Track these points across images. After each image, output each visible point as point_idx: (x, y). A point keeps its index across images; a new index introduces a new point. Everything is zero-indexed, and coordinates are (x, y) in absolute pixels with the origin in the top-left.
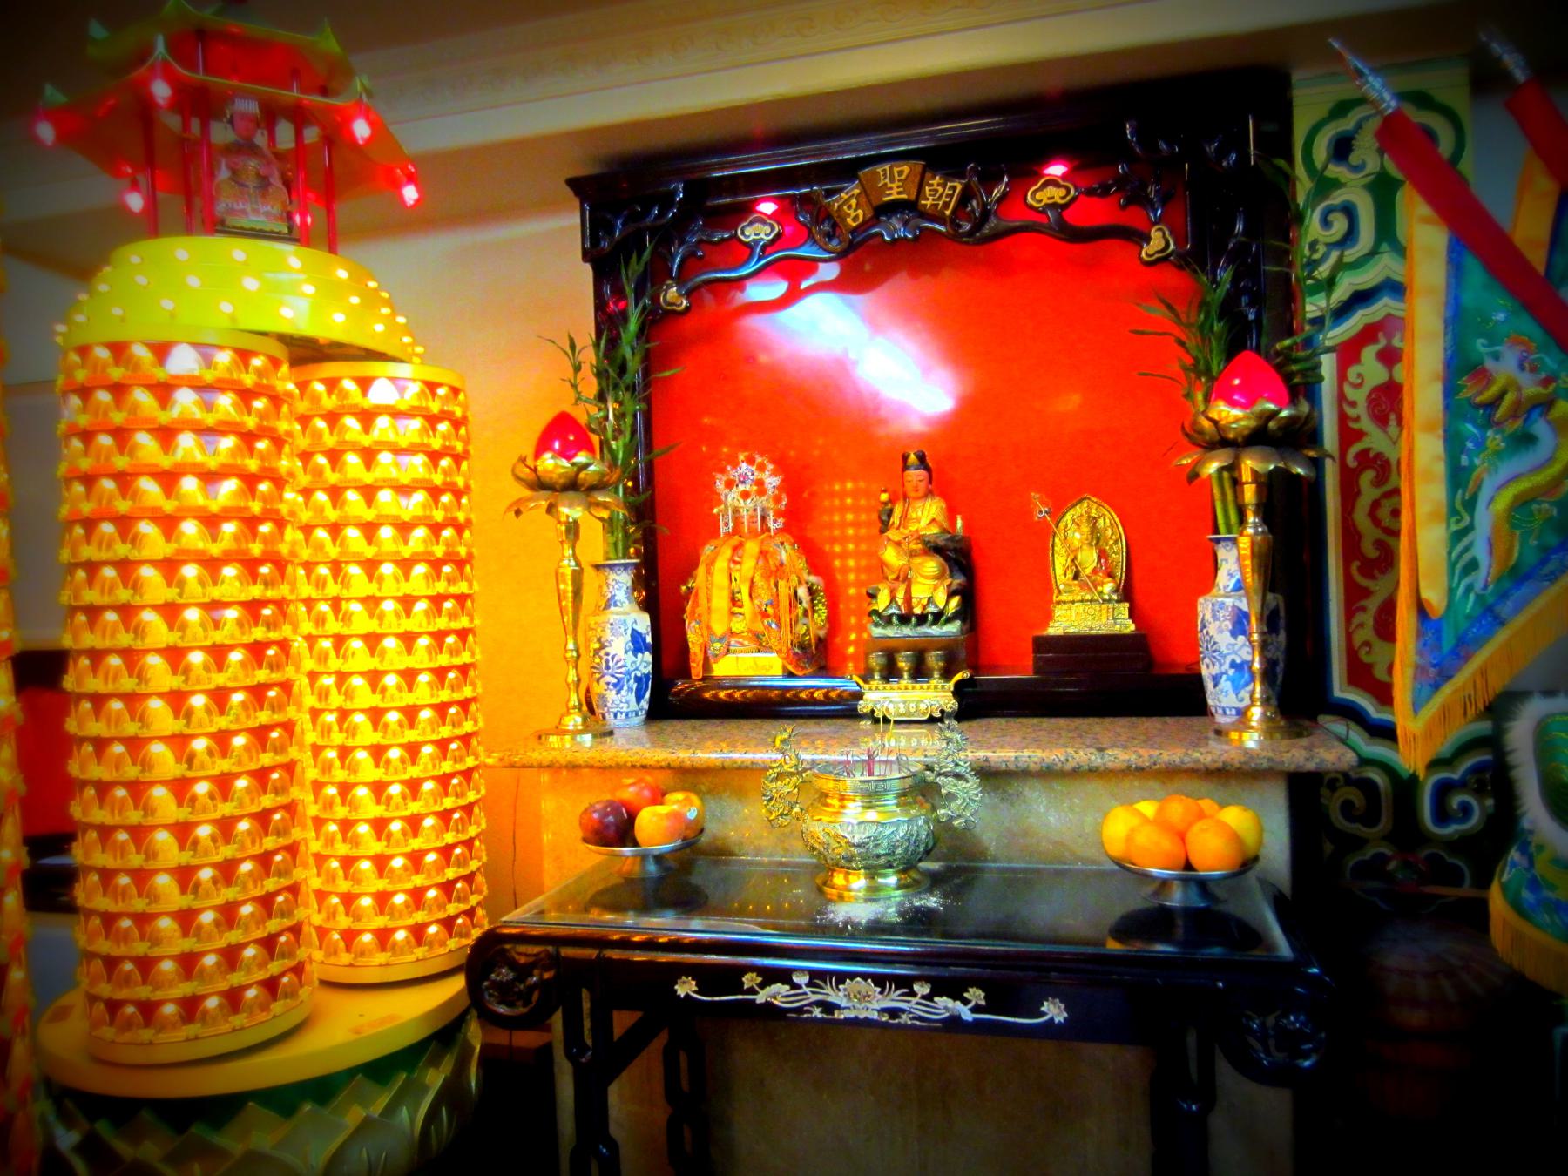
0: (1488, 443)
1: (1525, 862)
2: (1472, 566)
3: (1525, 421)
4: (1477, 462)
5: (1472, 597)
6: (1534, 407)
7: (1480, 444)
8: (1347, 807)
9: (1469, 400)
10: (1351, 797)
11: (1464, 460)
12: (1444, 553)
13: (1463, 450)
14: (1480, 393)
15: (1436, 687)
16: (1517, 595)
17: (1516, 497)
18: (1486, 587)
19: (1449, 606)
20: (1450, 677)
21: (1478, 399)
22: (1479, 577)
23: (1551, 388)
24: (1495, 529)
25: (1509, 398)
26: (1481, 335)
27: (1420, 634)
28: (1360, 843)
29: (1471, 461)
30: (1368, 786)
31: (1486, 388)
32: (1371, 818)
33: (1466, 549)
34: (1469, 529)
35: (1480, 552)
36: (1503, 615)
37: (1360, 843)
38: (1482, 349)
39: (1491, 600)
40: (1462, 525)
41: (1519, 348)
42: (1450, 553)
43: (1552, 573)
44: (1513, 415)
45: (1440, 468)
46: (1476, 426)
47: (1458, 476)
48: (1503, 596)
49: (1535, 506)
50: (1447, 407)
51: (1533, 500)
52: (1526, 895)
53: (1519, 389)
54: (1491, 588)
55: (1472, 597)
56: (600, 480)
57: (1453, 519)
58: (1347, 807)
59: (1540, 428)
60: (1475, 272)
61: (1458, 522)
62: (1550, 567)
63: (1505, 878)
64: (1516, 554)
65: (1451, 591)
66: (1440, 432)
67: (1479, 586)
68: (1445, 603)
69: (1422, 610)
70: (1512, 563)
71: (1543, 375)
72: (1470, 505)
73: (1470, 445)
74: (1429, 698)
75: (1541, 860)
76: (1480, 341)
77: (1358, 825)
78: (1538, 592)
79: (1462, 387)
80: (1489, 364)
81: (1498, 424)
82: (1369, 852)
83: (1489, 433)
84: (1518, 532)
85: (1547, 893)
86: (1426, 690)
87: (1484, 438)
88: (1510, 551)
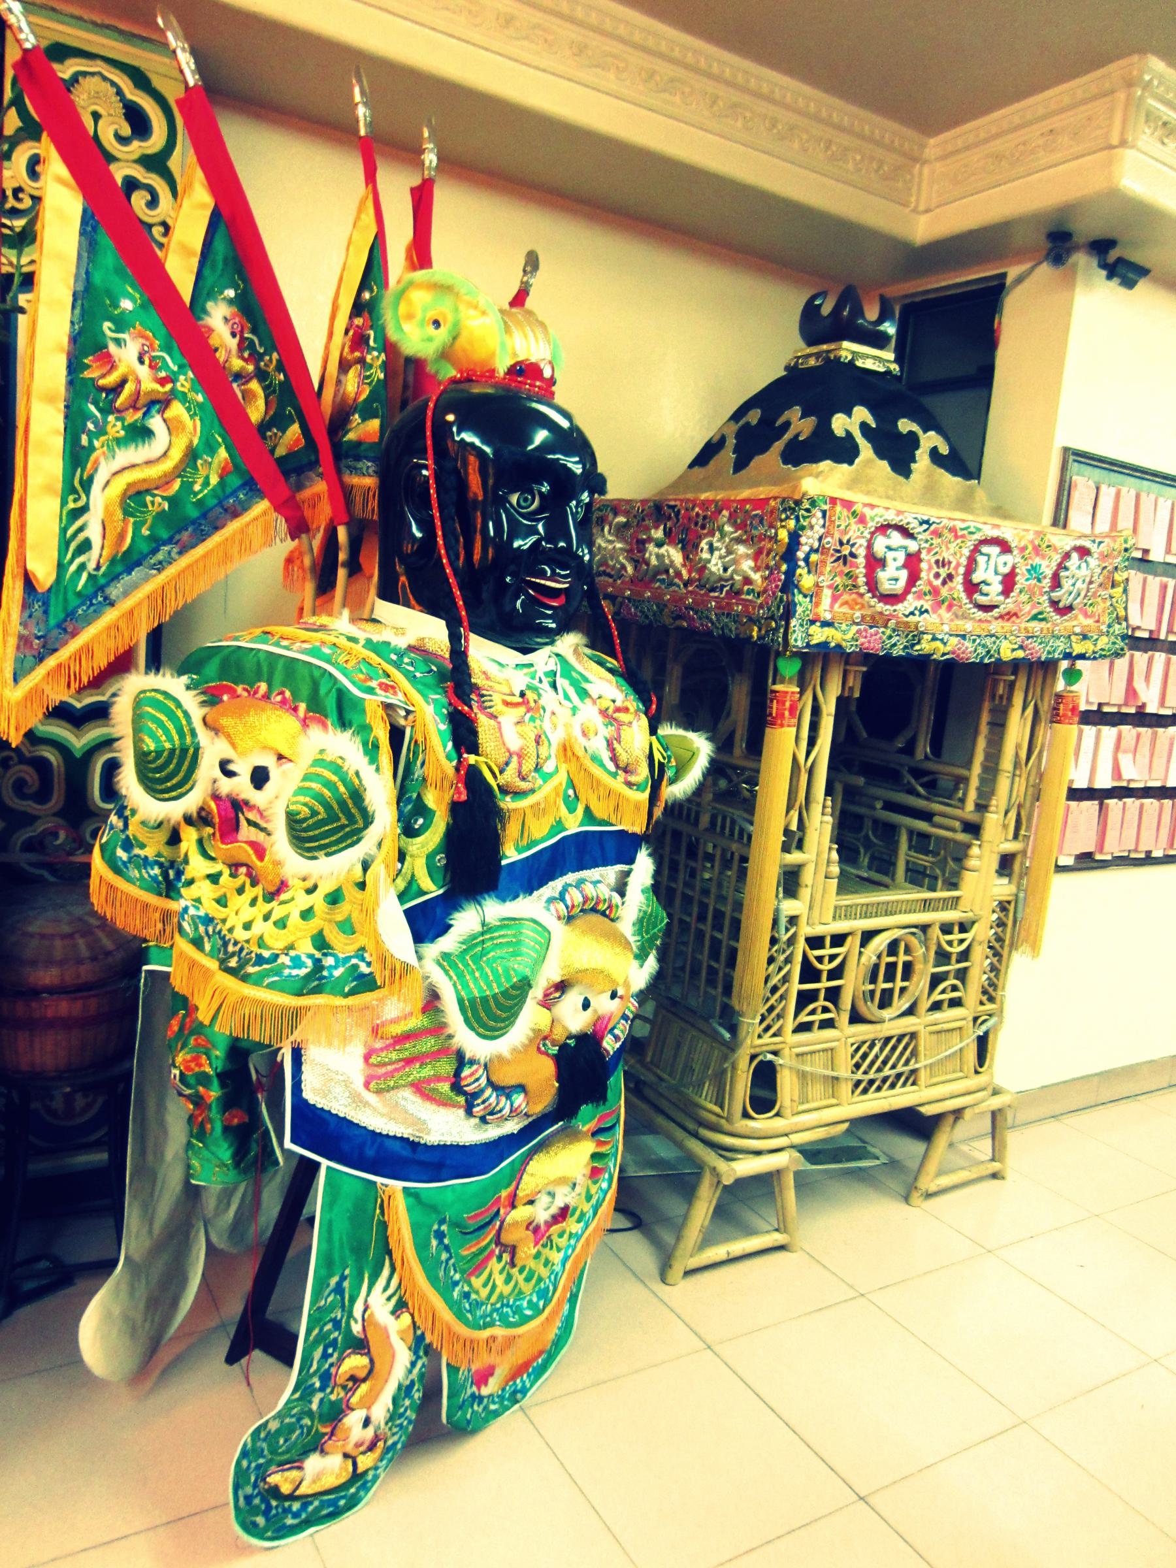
0: (109, 428)
1: (121, 825)
2: (86, 546)
3: (145, 414)
4: (96, 444)
5: (85, 576)
6: (153, 403)
7: (101, 430)
8: (19, 787)
9: (93, 379)
10: (28, 778)
11: (84, 440)
12: (56, 528)
13: (84, 430)
14: (103, 376)
15: (40, 659)
16: (126, 579)
17: (129, 485)
18: (98, 568)
19: (58, 580)
20: (55, 650)
21: (101, 382)
22: (91, 559)
23: (169, 387)
24: (108, 512)
25: (129, 388)
26: (110, 319)
27: (25, 606)
28: (31, 819)
29: (90, 442)
30: (42, 765)
31: (109, 372)
32: (43, 795)
33: (81, 529)
34: (85, 509)
35: (93, 532)
36: (113, 597)
37: (31, 819)
38: (109, 333)
39: (102, 581)
40: (80, 504)
41: (142, 341)
42: (64, 531)
43: (160, 563)
44: (133, 405)
45: (58, 442)
46: (100, 410)
47: (77, 457)
48: (114, 578)
49: (149, 498)
50: (70, 383)
51: (148, 491)
52: (121, 854)
53: (139, 382)
54: (103, 569)
55: (85, 576)
56: (475, 688)
57: (71, 498)
58: (19, 787)
59: (155, 423)
60: (109, 256)
61: (75, 501)
62: (160, 556)
63: (104, 840)
64: (128, 540)
65: (61, 567)
66: (62, 406)
67: (91, 566)
68: (53, 577)
69: (29, 582)
70: (125, 548)
71: (163, 374)
72: (87, 484)
73: (91, 426)
74: (32, 669)
75: (134, 822)
76: (107, 325)
77: (30, 803)
78: (147, 579)
79: (88, 367)
80: (112, 348)
81: (119, 411)
82: (40, 827)
83: (111, 418)
84: (132, 520)
85: (137, 851)
86: (30, 660)
87: (106, 422)
88: (121, 537)
